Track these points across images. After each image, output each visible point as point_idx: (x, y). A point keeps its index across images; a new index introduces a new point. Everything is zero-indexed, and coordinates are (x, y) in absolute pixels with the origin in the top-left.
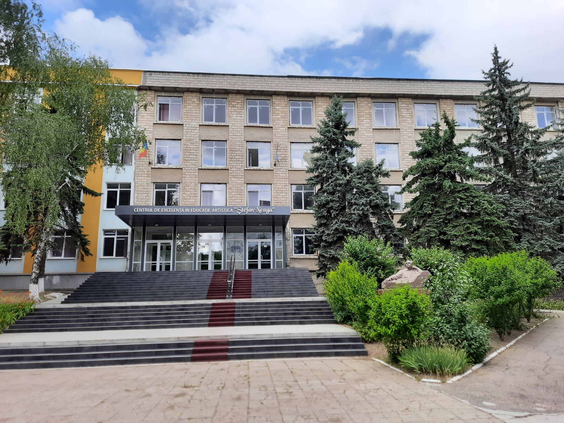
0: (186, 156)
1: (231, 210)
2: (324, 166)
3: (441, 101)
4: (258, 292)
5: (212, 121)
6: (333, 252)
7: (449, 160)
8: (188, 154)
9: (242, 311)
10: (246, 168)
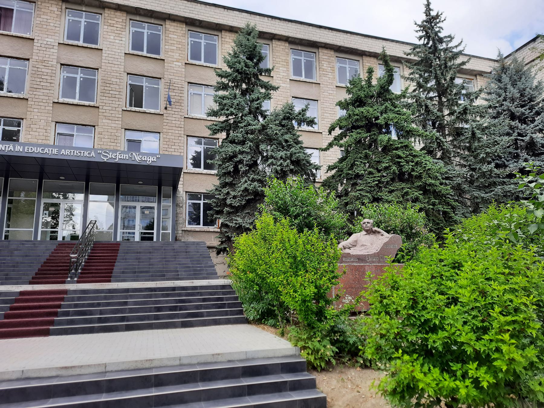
0: (35, 82)
1: (93, 154)
2: (232, 107)
3: (364, 58)
4: (123, 273)
5: (79, 40)
6: (240, 220)
7: (385, 111)
8: (38, 80)
9: (76, 306)
10: (125, 109)
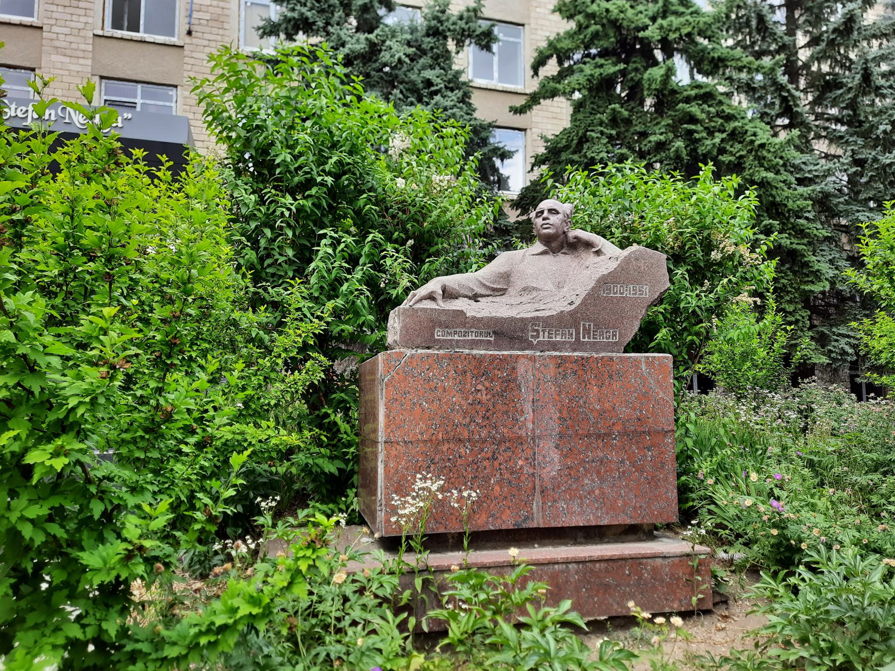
10: (100, 33)
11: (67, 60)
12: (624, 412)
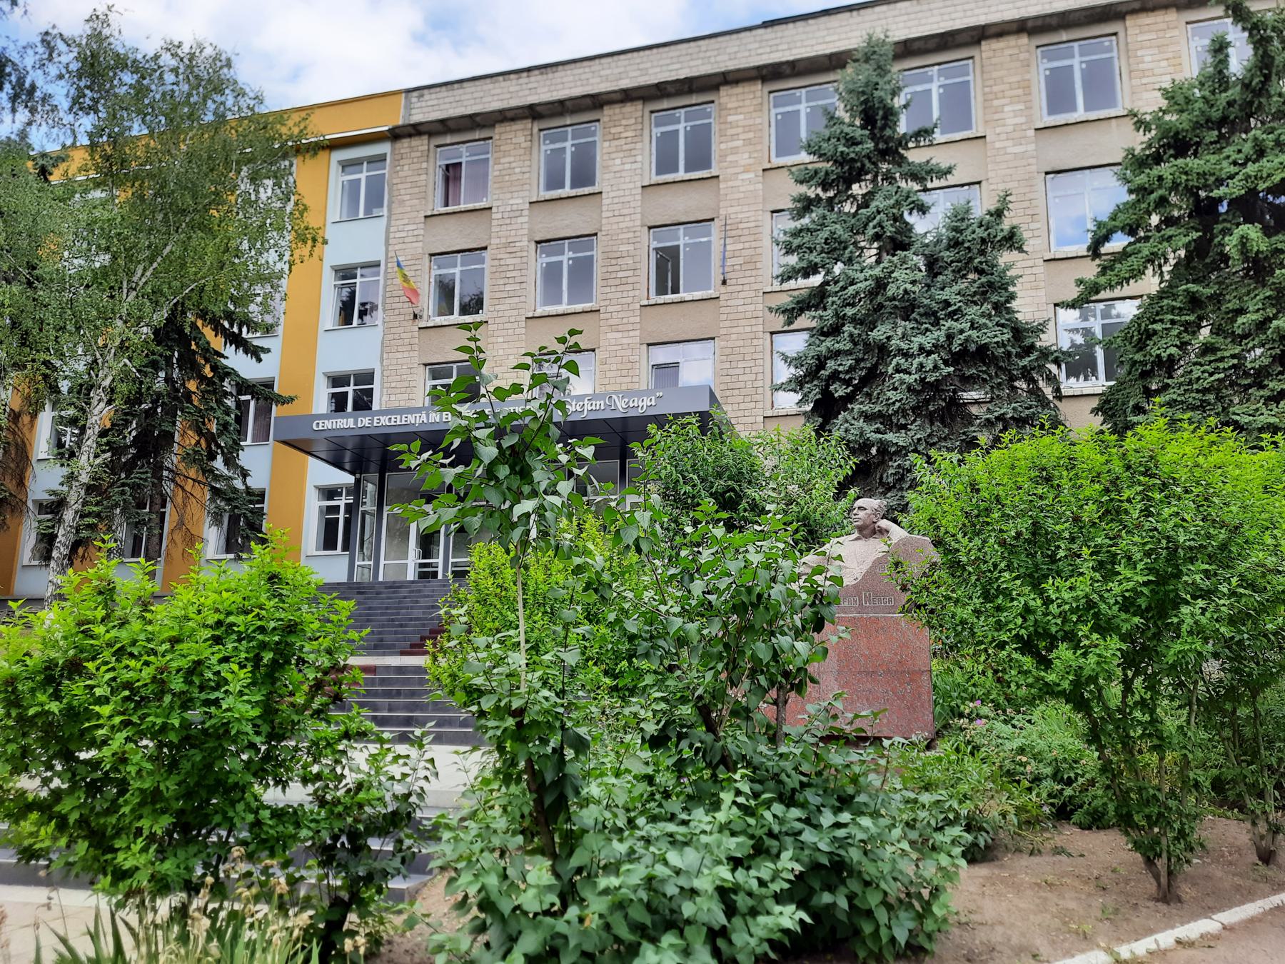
11: (620, 335)
12: (887, 656)
